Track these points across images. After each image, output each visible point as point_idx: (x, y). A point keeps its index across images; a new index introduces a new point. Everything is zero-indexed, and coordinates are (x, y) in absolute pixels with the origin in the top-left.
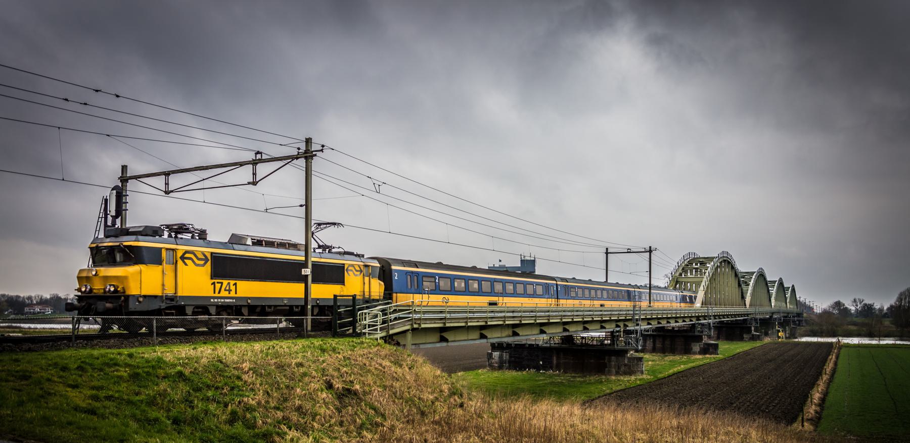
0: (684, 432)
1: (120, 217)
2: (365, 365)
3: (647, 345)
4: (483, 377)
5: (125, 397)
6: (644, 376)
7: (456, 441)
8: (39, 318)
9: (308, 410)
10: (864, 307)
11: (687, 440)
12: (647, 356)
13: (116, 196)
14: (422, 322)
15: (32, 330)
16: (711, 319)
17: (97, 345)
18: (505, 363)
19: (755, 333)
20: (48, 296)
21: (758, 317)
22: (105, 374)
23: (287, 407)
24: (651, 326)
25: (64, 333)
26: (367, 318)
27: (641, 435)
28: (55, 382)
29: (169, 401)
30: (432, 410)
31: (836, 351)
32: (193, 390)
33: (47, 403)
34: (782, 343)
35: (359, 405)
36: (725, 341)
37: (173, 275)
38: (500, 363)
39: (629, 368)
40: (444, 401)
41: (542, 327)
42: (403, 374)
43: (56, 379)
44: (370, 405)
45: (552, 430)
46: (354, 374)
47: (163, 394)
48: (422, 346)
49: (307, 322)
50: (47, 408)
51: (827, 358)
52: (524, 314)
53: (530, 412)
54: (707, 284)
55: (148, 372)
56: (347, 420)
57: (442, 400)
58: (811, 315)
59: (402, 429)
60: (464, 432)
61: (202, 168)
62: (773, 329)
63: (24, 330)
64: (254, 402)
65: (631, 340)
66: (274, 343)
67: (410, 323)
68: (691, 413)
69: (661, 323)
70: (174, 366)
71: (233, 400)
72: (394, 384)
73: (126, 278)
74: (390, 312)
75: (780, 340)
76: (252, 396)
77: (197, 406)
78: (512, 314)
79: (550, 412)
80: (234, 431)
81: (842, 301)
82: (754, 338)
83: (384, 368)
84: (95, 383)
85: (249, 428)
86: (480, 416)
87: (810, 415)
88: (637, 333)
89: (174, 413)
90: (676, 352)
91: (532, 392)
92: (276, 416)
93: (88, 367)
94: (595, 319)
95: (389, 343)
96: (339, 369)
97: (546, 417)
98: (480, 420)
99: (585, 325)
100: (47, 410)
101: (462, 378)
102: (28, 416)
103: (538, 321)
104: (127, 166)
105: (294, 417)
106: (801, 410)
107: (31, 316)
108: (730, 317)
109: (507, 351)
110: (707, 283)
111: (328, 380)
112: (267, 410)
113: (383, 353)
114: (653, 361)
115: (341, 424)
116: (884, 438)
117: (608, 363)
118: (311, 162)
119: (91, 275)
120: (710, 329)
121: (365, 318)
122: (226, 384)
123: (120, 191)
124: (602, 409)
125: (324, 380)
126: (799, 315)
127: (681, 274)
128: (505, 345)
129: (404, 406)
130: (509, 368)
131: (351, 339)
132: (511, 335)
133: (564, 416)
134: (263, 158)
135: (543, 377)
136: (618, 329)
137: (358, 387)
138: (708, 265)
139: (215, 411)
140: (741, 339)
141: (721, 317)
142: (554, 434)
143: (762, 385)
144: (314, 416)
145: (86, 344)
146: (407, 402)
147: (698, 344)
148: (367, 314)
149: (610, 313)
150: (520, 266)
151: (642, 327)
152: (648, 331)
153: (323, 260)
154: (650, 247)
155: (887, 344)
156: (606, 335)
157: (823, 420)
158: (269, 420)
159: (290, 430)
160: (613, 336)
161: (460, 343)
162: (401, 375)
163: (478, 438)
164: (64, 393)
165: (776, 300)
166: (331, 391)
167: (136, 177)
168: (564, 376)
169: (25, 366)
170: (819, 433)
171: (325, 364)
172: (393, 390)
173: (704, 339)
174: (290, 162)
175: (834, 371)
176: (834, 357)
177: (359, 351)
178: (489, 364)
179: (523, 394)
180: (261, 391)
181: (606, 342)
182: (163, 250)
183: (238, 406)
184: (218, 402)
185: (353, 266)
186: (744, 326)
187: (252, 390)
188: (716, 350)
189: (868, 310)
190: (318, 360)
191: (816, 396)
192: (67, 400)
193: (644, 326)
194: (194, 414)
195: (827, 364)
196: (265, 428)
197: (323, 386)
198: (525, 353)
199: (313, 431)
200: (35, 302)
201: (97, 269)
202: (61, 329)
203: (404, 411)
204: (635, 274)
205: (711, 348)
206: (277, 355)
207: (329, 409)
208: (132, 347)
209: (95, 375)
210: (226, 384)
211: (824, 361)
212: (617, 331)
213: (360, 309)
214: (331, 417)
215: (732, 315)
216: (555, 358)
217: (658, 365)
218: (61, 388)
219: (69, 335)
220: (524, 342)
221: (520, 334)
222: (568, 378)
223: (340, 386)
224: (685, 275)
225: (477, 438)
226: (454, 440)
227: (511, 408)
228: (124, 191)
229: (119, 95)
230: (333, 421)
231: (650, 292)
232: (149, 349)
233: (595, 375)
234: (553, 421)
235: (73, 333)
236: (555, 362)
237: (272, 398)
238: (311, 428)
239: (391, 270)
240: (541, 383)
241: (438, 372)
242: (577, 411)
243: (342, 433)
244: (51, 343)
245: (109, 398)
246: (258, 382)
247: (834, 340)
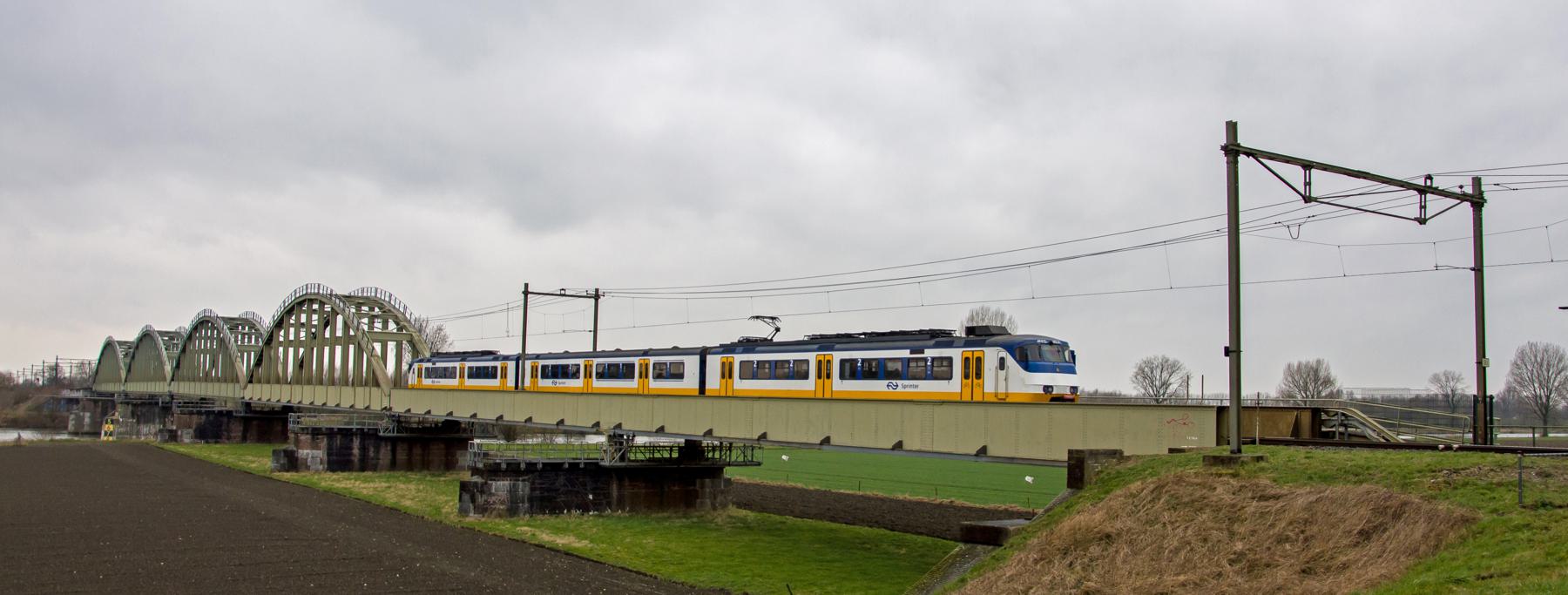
3: (381, 457)
18: (523, 502)
38: (512, 502)
109: (526, 478)
117: (700, 490)
130: (531, 511)
154: (597, 290)
198: (562, 480)
216: (615, 485)
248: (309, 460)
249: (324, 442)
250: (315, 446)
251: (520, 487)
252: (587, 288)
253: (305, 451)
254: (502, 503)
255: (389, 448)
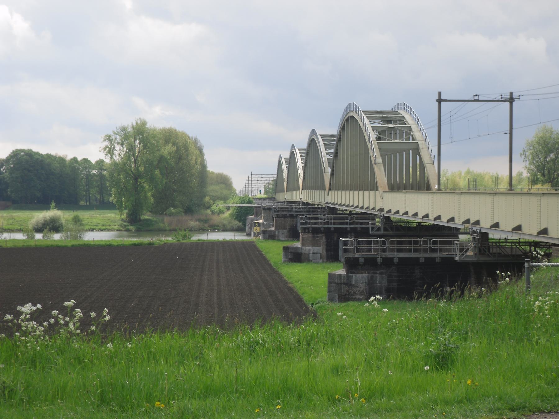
109: (384, 271)
154: (511, 94)
248: (311, 255)
249: (323, 240)
250: (315, 244)
251: (378, 279)
253: (308, 248)
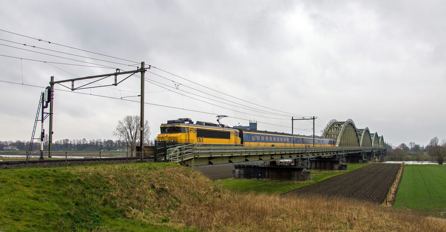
0: (330, 208)
1: (50, 102)
2: (171, 176)
4: (230, 182)
5: (52, 192)
6: (311, 181)
7: (217, 214)
8: (11, 153)
9: (142, 199)
10: (415, 146)
11: (332, 212)
12: (312, 171)
13: (48, 92)
14: (200, 155)
15: (7, 158)
16: (343, 152)
17: (38, 166)
18: (242, 175)
19: (364, 159)
20: (15, 141)
21: (366, 151)
22: (42, 180)
23: (132, 197)
24: (314, 156)
25: (23, 160)
26: (172, 153)
27: (310, 210)
28: (18, 184)
29: (74, 194)
30: (205, 199)
31: (402, 168)
32: (85, 188)
33: (15, 195)
34: (377, 164)
35: (168, 196)
36: (350, 163)
37: (188, 136)
38: (239, 175)
39: (304, 177)
40: (211, 194)
41: (260, 157)
42: (190, 181)
43: (19, 182)
44: (173, 197)
45: (265, 208)
46: (165, 181)
47: (71, 190)
48: (199, 167)
49: (141, 154)
50: (14, 197)
51: (398, 171)
52: (251, 151)
53: (254, 199)
54: (341, 135)
55: (63, 179)
56: (162, 204)
57: (210, 194)
58: (390, 150)
59: (189, 208)
60: (221, 210)
61: (90, 77)
62: (373, 157)
63: (3, 158)
64: (115, 195)
65: (305, 163)
66: (125, 165)
67: (194, 155)
68: (334, 199)
69: (319, 155)
70: (76, 176)
71: (105, 193)
72: (186, 186)
73: (177, 137)
74: (183, 149)
75: (376, 163)
76: (114, 191)
77: (87, 196)
78: (245, 150)
79: (264, 200)
80: (106, 209)
81: (405, 143)
82: (364, 162)
83: (180, 178)
84: (38, 185)
85: (113, 208)
86: (229, 202)
87: (390, 199)
88: (307, 159)
89: (76, 200)
90: (327, 169)
91: (255, 189)
92: (126, 202)
93: (34, 177)
94: (287, 153)
95: (183, 165)
96: (158, 178)
97: (262, 202)
98: (229, 204)
99: (282, 156)
100: (15, 198)
101: (220, 183)
102: (5, 201)
103: (258, 154)
104: (53, 77)
105: (136, 202)
106: (386, 197)
107: (6, 151)
108: (352, 151)
109: (243, 169)
110: (341, 135)
111: (152, 184)
112: (122, 199)
113: (180, 170)
114: (315, 173)
115: (159, 206)
116: (424, 210)
118: (144, 74)
119: (164, 136)
120: (343, 158)
121: (171, 152)
122: (101, 186)
123: (50, 89)
124: (290, 198)
125: (150, 184)
126: (385, 150)
127: (329, 130)
128: (241, 166)
129: (191, 197)
130: (244, 178)
131: (164, 163)
132: (245, 161)
133: (271, 201)
134: (120, 72)
135: (261, 182)
136: (298, 158)
137: (167, 187)
138: (342, 126)
139: (96, 199)
140: (358, 162)
141: (348, 151)
142: (266, 211)
143: (368, 185)
144: (145, 202)
145: (33, 165)
146: (192, 195)
147: (337, 165)
148: (172, 150)
149: (294, 150)
150: (249, 126)
151: (310, 157)
152: (313, 159)
153: (224, 130)
154: (314, 117)
155: (425, 164)
156: (292, 161)
157: (396, 201)
158: (123, 204)
159: (133, 209)
160: (295, 161)
161: (217, 164)
162: (189, 181)
163: (228, 213)
164: (23, 189)
165: (374, 143)
166: (153, 189)
167: (58, 82)
168: (271, 182)
169: (4, 176)
170: (394, 208)
171: (150, 176)
172: (185, 189)
173: (340, 163)
174: (133, 74)
175: (401, 177)
176: (401, 171)
177: (168, 169)
178: (233, 176)
179: (251, 190)
180: (119, 189)
181: (292, 164)
182: (186, 128)
183: (107, 197)
184: (98, 195)
185: (232, 132)
186: (359, 156)
187: (114, 188)
188: (346, 168)
189: (417, 148)
190: (147, 174)
191: (393, 190)
192: (24, 193)
193: (311, 156)
194: (86, 200)
195: (398, 174)
196: (121, 208)
197: (149, 187)
198: (252, 170)
199: (145, 209)
200: (8, 144)
201: (167, 134)
202: (21, 158)
203: (191, 200)
204: (307, 130)
205: (343, 167)
206: (126, 171)
207: (153, 198)
208: (55, 167)
209: (38, 181)
210: (101, 186)
211: (397, 173)
212: (298, 159)
213: (168, 148)
214: (154, 202)
215: (354, 150)
216: (267, 172)
217: (318, 175)
218: (21, 187)
219: (25, 161)
220: (251, 165)
221: (249, 161)
222: (273, 182)
223: (158, 187)
224: (331, 131)
225: (227, 213)
226: (216, 214)
227: (244, 198)
228: (52, 89)
229: (403, 172)
230: (155, 204)
231: (314, 139)
232: (64, 168)
233: (287, 181)
234: (266, 204)
235: (27, 160)
236: (267, 174)
237: (124, 193)
238: (144, 208)
239: (243, 133)
240: (260, 185)
241: (208, 180)
242: (278, 199)
243: (159, 211)
244: (16, 165)
245: (44, 192)
246: (117, 184)
247: (401, 162)
252: (311, 116)
254: (237, 175)
255: (315, 163)
